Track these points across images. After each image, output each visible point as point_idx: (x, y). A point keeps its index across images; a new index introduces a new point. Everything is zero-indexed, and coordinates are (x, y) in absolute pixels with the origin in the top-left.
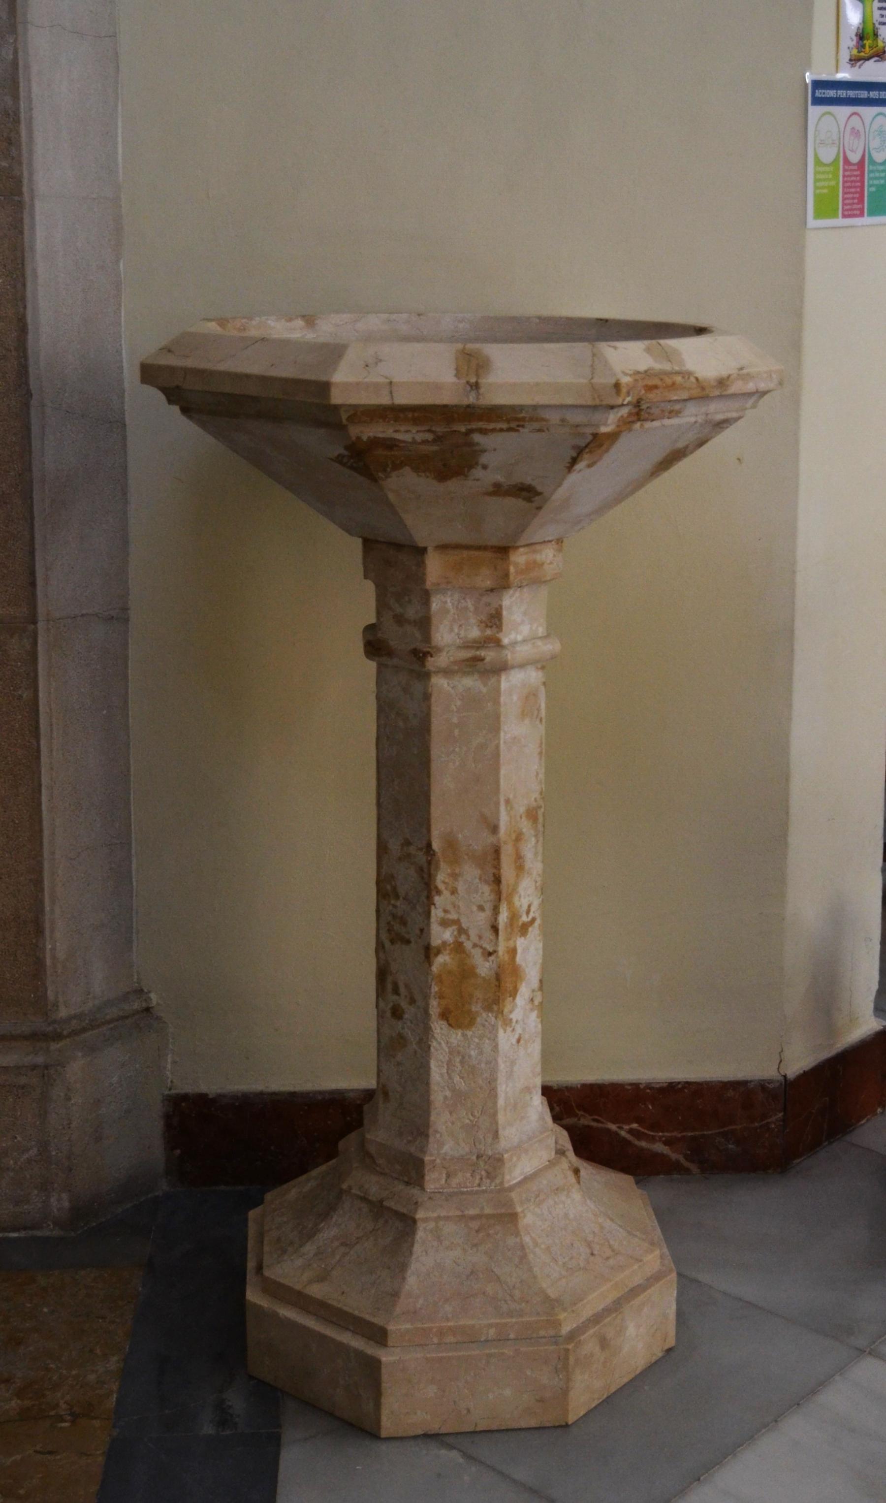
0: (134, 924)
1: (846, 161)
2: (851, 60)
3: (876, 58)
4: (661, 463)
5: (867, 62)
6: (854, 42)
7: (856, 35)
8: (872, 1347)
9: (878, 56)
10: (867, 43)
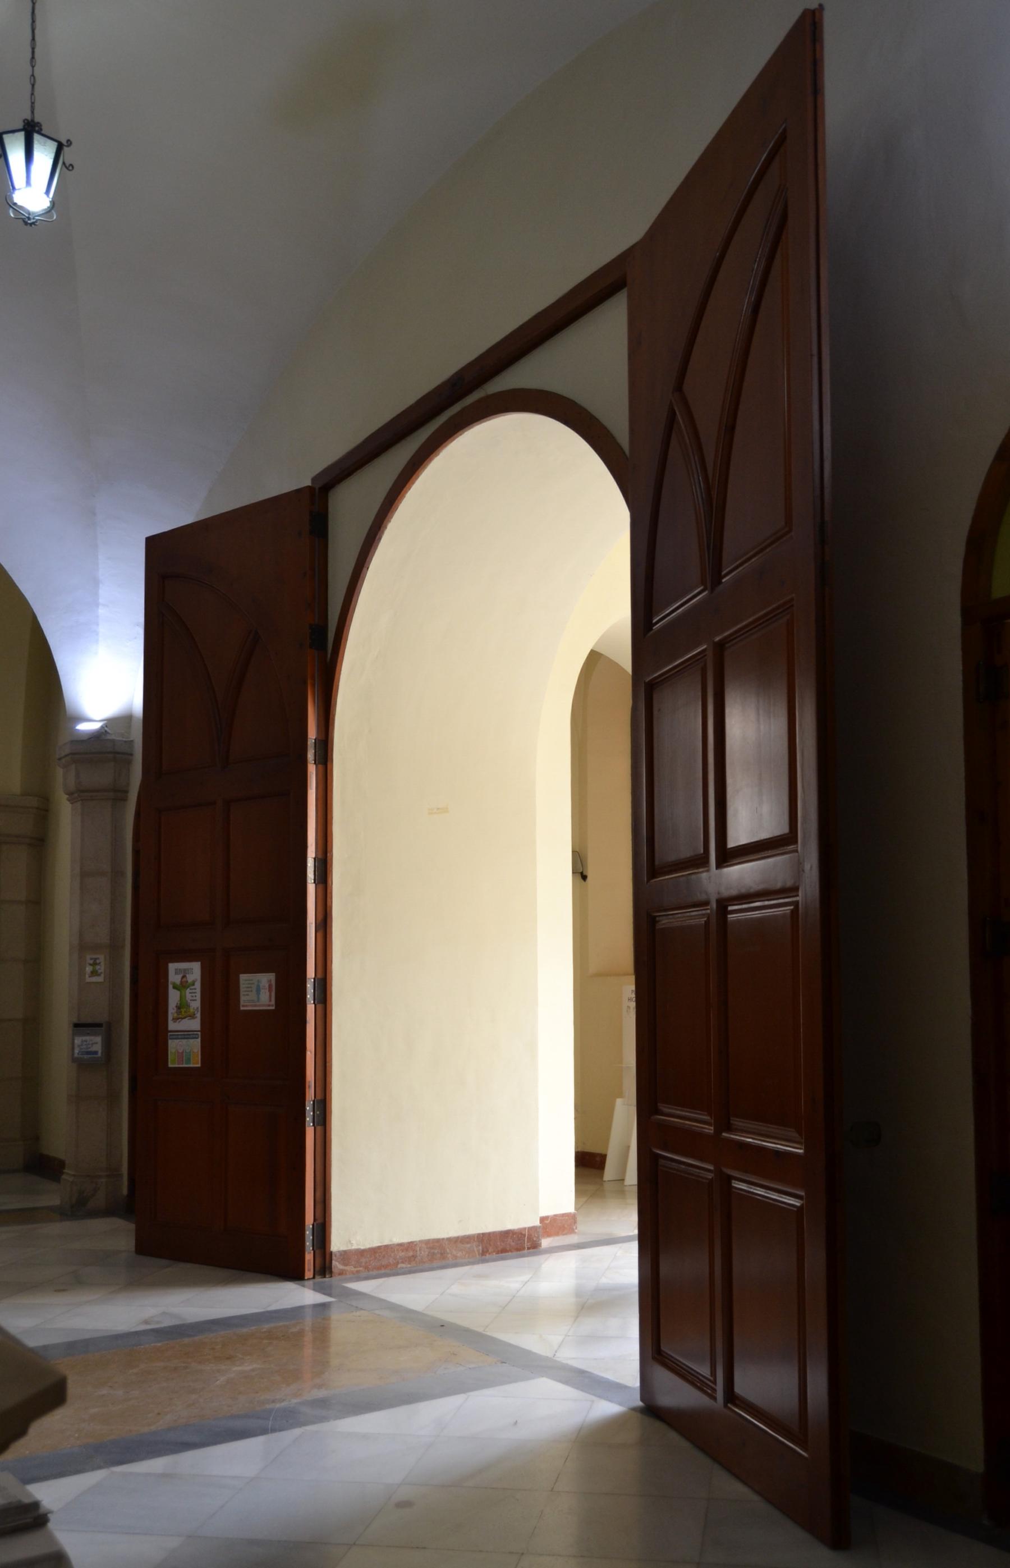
0: (760, 253)
1: (178, 1052)
2: (173, 1019)
3: (189, 1018)
4: (582, 1372)
5: (184, 1020)
6: (175, 1010)
7: (176, 1007)
8: (710, 1130)
9: (190, 1016)
10: (183, 1010)
